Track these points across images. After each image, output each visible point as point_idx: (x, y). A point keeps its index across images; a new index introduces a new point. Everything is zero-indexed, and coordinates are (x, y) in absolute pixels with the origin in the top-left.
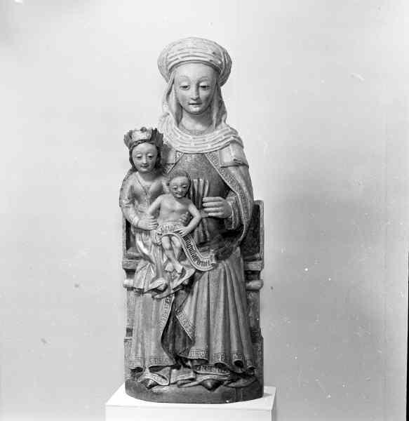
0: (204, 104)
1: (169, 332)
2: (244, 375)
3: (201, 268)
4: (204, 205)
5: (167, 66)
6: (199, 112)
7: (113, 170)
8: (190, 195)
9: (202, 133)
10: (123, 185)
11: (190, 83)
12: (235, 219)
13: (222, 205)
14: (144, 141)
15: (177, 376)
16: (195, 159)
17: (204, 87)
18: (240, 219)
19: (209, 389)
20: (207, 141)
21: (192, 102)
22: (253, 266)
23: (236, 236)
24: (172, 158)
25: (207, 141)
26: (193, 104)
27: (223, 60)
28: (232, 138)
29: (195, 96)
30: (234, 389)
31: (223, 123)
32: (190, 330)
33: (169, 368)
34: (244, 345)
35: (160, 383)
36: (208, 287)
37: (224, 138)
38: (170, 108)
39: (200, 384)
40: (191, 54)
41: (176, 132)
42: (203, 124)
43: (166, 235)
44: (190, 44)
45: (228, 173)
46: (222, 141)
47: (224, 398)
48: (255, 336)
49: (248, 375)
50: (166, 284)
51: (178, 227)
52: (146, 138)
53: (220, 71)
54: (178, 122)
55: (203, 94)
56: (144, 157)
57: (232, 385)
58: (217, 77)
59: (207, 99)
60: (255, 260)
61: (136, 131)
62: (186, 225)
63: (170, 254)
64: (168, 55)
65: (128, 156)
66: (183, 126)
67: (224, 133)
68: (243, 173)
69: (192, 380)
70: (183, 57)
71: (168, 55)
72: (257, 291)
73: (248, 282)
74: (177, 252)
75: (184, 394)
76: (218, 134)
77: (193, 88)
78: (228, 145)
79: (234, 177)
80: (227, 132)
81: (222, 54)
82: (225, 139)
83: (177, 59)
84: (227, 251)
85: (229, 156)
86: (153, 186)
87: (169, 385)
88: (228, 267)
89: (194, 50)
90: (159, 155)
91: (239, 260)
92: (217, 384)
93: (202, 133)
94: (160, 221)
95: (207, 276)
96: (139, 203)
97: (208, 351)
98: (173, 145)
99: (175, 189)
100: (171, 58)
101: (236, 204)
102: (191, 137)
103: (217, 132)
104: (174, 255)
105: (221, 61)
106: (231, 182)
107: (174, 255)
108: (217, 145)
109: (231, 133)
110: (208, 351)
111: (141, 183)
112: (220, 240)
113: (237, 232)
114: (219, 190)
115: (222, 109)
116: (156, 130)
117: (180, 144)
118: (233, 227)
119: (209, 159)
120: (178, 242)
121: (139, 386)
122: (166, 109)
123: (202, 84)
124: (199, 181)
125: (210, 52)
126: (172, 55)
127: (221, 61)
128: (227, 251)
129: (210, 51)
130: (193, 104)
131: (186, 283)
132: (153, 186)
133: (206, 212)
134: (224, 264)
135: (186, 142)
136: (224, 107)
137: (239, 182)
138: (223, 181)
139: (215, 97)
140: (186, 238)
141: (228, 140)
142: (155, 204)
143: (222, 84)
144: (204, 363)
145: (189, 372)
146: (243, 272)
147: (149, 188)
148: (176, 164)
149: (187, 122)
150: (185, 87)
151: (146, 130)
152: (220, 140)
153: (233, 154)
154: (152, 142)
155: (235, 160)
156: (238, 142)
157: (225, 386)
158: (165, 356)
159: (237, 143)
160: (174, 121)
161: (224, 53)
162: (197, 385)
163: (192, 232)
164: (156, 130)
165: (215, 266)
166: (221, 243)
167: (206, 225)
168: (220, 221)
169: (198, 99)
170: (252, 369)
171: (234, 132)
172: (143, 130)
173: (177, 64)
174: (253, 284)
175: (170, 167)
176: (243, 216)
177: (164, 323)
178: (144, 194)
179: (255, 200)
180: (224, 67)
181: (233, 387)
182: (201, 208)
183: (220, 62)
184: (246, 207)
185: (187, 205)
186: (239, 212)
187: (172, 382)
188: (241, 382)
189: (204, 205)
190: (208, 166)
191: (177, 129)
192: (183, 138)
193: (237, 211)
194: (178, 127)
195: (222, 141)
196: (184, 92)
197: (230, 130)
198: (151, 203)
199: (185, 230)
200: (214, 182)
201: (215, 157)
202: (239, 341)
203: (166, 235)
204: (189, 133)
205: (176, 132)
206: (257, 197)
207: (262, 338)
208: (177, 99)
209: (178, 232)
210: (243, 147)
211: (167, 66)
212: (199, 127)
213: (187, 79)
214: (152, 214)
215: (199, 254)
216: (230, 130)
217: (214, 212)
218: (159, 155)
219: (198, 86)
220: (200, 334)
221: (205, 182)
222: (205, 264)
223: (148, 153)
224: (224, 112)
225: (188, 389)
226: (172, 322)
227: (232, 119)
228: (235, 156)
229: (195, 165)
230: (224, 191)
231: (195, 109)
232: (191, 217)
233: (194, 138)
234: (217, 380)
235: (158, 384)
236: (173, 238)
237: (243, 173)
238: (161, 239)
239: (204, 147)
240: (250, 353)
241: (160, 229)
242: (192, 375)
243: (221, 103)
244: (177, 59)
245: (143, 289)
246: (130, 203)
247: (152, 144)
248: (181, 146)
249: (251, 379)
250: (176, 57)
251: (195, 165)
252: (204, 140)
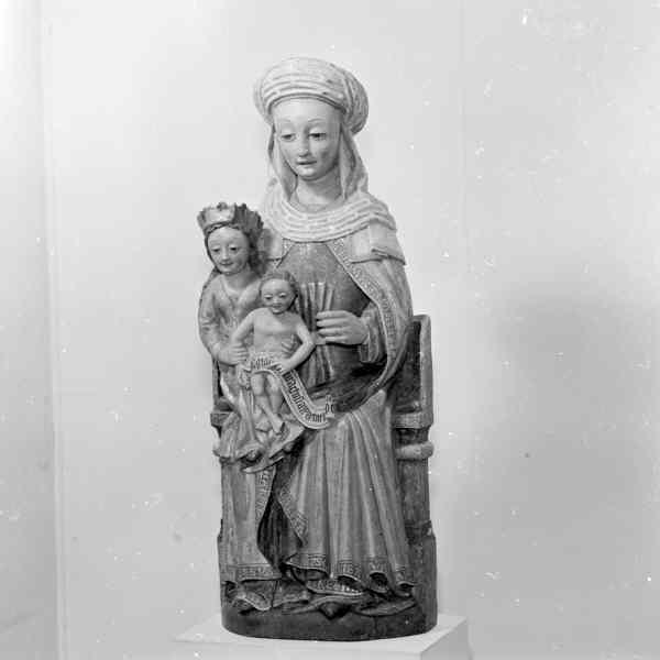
0: (319, 164)
2: (392, 597)
3: (311, 424)
4: (319, 324)
5: (264, 105)
6: (314, 175)
8: (297, 305)
9: (323, 208)
10: (203, 294)
11: (294, 129)
12: (374, 346)
14: (223, 224)
15: (286, 597)
16: (311, 251)
17: (317, 135)
18: (383, 345)
19: (330, 618)
20: (329, 221)
21: (300, 160)
22: (409, 421)
23: (382, 372)
24: (276, 251)
25: (329, 221)
26: (302, 164)
27: (346, 91)
28: (372, 216)
29: (302, 151)
30: (372, 619)
31: (359, 191)
33: (272, 584)
34: (391, 545)
35: (257, 607)
36: (324, 455)
37: (357, 215)
38: (276, 171)
40: (294, 83)
41: (284, 208)
42: (326, 195)
43: (256, 373)
44: (290, 68)
46: (355, 221)
47: (356, 635)
48: (417, 532)
49: (400, 597)
50: (259, 452)
51: (276, 359)
52: (225, 219)
53: (346, 112)
54: (289, 192)
55: (316, 146)
56: (224, 249)
57: (369, 612)
58: (342, 119)
59: (324, 154)
60: (412, 411)
61: (209, 208)
62: (289, 355)
63: (263, 401)
64: (262, 87)
65: (205, 250)
66: (296, 197)
67: (358, 209)
68: (390, 272)
69: (305, 602)
70: (282, 90)
71: (262, 87)
72: (422, 462)
73: (400, 447)
74: (275, 400)
76: (348, 210)
77: (300, 137)
78: (366, 227)
79: (373, 280)
80: (365, 206)
81: (344, 82)
82: (360, 217)
83: (274, 93)
85: (363, 246)
86: (246, 294)
87: (271, 609)
88: (365, 421)
89: (298, 78)
90: (252, 246)
91: (382, 413)
92: (343, 610)
93: (323, 208)
94: (252, 352)
95: (321, 439)
96: (226, 322)
97: (327, 559)
98: (279, 229)
99: (268, 298)
100: (267, 91)
101: (376, 321)
102: (305, 215)
103: (347, 207)
104: (270, 404)
105: (343, 93)
107: (270, 404)
108: (347, 227)
109: (371, 208)
110: (327, 559)
111: (226, 290)
112: (349, 381)
113: (374, 369)
114: (349, 300)
115: (357, 167)
116: (244, 206)
117: (288, 228)
118: (370, 360)
119: (333, 249)
120: (275, 383)
121: (243, 621)
122: (272, 172)
123: (312, 132)
124: (316, 286)
125: (322, 79)
126: (267, 86)
127: (343, 93)
128: (356, 398)
129: (322, 77)
130: (302, 164)
132: (246, 294)
133: (323, 336)
135: (296, 225)
136: (362, 166)
138: (356, 285)
139: (342, 151)
140: (287, 376)
141: (366, 219)
143: (356, 129)
145: (301, 591)
146: (388, 431)
147: (237, 299)
148: (283, 259)
149: (304, 193)
150: (288, 137)
151: (226, 207)
154: (236, 225)
155: (374, 251)
156: (388, 225)
159: (383, 224)
160: (283, 192)
161: (347, 81)
162: (311, 611)
163: (299, 368)
164: (244, 206)
165: (333, 422)
166: (349, 385)
167: (328, 355)
168: (352, 349)
169: (307, 155)
170: (405, 587)
171: (378, 205)
173: (275, 100)
174: (411, 450)
175: (274, 265)
176: (388, 341)
179: (415, 314)
180: (350, 103)
181: (369, 616)
182: (313, 327)
183: (340, 96)
184: (393, 326)
185: (294, 324)
186: (381, 334)
187: (275, 605)
188: (385, 609)
190: (331, 261)
191: (287, 204)
193: (376, 331)
194: (289, 199)
195: (355, 221)
196: (287, 145)
197: (369, 203)
198: (240, 321)
199: (286, 364)
200: (342, 288)
202: (380, 535)
203: (256, 373)
204: (303, 209)
205: (284, 208)
206: (416, 312)
207: (433, 537)
208: (281, 153)
209: (275, 366)
210: (393, 229)
211: (264, 105)
212: (321, 201)
213: (289, 124)
214: (242, 340)
215: (308, 402)
216: (369, 203)
217: (334, 335)
218: (252, 246)
219: (307, 135)
220: (316, 533)
221: (326, 288)
222: (318, 418)
223: (231, 242)
224: (362, 175)
228: (375, 245)
229: (311, 261)
230: (358, 302)
231: (305, 171)
233: (309, 218)
236: (269, 377)
237: (390, 272)
238: (249, 379)
239: (325, 231)
240: (402, 560)
241: (249, 364)
242: (305, 596)
243: (354, 160)
244: (274, 93)
245: (229, 458)
246: (211, 323)
247: (237, 228)
248: (291, 231)
249: (404, 603)
250: (272, 91)
251: (311, 261)
252: (325, 221)
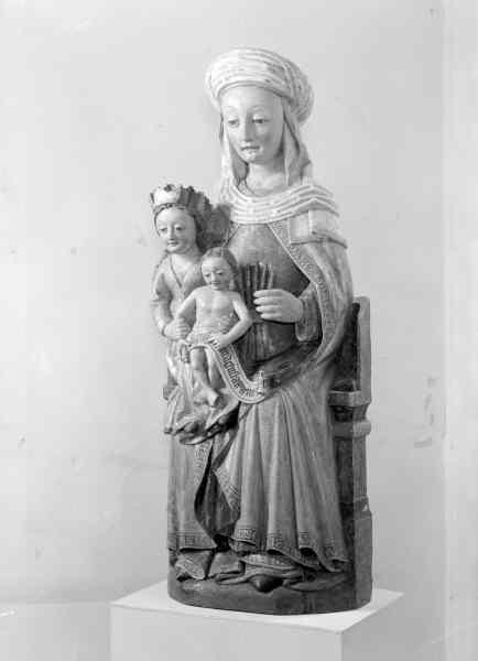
1: (206, 497)
7: (147, 246)
8: (245, 281)
13: (280, 301)
17: (260, 121)
26: (247, 148)
32: (232, 496)
37: (298, 199)
39: (247, 581)
43: (196, 348)
45: (302, 253)
46: (297, 204)
47: (283, 608)
48: (350, 506)
62: (226, 331)
67: (301, 192)
75: (225, 596)
79: (314, 262)
82: (302, 201)
84: (290, 374)
85: (305, 227)
87: (205, 579)
92: (271, 583)
106: (308, 267)
131: (221, 422)
134: (292, 393)
137: (321, 268)
142: (189, 298)
144: (256, 544)
147: (183, 277)
152: (293, 203)
153: (311, 225)
157: (286, 586)
158: (202, 533)
172: (169, 188)
177: (197, 483)
178: (177, 285)
189: (256, 302)
192: (240, 201)
194: (237, 186)
195: (297, 204)
201: (283, 229)
203: (196, 348)
206: (357, 294)
209: (211, 342)
225: (230, 588)
226: (209, 482)
227: (319, 173)
228: (314, 227)
232: (236, 318)
233: (254, 202)
234: (272, 577)
235: (190, 577)
